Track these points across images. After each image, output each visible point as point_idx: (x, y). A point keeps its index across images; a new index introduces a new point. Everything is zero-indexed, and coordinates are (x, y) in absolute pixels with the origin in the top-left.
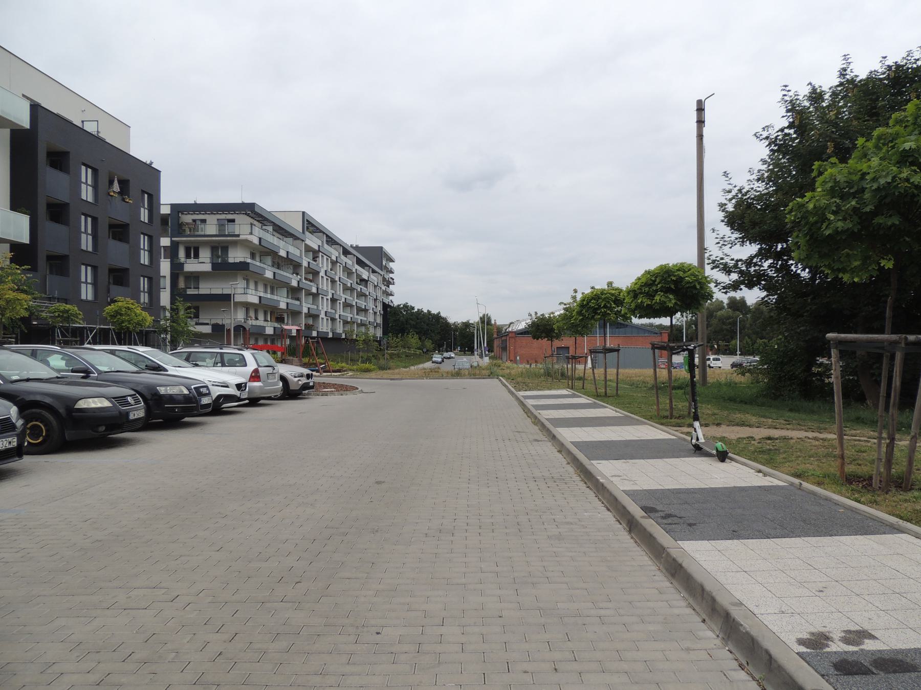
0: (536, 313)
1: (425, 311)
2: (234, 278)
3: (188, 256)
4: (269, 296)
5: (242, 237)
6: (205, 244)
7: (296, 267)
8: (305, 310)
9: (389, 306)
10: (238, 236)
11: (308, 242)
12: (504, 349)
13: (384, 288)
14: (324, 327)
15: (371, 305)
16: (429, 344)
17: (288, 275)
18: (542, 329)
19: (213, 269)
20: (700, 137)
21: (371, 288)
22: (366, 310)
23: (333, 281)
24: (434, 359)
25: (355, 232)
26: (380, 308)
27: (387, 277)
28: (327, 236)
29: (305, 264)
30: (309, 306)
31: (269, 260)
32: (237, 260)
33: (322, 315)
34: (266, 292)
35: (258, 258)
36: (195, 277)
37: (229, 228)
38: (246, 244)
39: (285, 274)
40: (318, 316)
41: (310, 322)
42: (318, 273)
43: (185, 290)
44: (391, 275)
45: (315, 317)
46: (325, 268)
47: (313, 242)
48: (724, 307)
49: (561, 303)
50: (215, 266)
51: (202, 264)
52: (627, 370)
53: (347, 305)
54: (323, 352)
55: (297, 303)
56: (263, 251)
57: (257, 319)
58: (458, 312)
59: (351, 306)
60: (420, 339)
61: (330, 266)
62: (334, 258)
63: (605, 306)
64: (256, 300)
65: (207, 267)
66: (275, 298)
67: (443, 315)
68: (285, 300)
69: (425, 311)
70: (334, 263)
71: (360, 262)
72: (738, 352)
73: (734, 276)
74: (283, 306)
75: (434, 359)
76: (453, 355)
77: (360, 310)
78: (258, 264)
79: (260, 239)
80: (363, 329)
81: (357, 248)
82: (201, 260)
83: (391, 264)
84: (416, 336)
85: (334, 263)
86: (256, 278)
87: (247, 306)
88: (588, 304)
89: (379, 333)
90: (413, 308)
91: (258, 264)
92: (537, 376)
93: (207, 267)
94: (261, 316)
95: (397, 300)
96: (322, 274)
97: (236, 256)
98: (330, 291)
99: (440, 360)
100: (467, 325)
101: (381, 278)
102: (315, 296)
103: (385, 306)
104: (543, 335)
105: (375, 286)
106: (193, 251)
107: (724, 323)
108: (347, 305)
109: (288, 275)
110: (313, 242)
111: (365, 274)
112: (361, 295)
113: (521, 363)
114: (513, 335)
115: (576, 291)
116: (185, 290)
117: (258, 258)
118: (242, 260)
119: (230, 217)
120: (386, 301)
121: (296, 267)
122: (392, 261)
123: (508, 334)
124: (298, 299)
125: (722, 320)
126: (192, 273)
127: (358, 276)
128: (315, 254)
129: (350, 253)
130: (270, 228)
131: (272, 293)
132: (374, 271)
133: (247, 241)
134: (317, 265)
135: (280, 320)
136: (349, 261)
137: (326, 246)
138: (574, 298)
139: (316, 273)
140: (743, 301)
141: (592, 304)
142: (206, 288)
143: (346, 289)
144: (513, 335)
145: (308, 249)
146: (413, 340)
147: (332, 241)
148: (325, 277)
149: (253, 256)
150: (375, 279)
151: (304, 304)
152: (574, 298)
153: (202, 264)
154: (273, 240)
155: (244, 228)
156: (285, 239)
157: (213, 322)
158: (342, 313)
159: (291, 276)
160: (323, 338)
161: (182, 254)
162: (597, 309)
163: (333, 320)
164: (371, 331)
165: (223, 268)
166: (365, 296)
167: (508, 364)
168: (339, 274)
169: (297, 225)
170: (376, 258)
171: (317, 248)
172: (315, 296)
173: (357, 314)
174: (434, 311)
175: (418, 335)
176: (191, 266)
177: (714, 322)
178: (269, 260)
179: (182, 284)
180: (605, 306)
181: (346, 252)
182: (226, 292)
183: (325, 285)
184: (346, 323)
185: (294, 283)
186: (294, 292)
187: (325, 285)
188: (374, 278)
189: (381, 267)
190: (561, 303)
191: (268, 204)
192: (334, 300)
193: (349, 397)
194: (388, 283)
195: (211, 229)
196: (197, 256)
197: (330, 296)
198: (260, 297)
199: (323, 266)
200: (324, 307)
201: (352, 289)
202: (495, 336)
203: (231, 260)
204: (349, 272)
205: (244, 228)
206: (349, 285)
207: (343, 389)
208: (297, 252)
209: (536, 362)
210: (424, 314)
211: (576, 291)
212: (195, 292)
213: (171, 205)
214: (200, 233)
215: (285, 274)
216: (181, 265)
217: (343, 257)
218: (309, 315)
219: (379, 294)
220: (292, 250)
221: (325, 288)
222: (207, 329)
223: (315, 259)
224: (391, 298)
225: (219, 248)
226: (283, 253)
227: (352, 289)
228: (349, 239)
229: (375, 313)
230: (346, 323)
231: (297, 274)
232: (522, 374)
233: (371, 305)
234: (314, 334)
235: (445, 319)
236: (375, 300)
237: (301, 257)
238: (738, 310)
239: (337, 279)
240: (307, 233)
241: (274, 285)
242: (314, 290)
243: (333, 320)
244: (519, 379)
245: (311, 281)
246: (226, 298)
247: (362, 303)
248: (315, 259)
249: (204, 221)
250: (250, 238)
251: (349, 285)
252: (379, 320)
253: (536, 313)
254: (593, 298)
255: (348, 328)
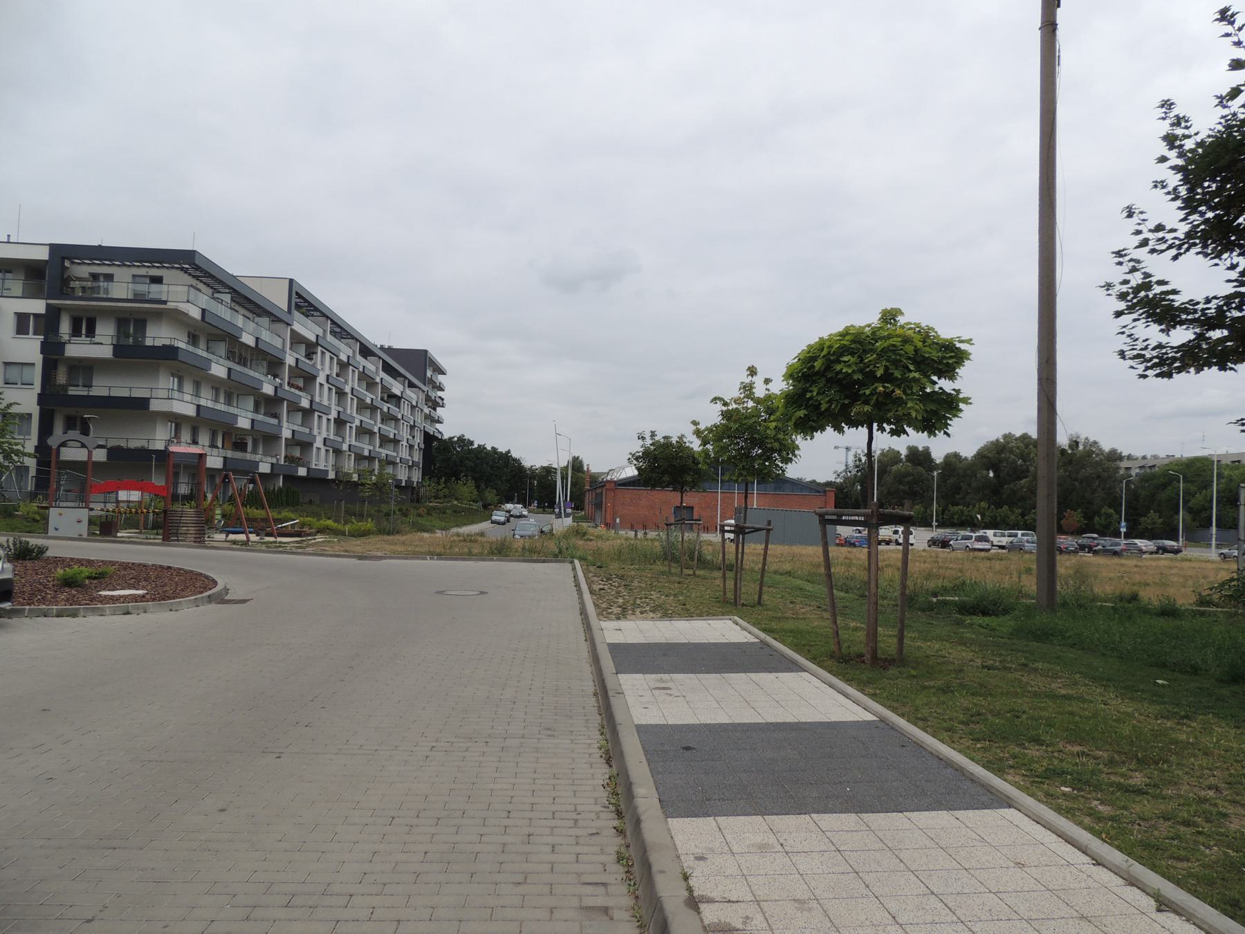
0: (653, 434)
1: (489, 448)
2: (152, 371)
3: (76, 332)
4: (221, 407)
5: (170, 305)
6: (107, 313)
7: (274, 365)
8: (286, 433)
9: (433, 438)
10: (165, 302)
11: (297, 327)
12: (598, 505)
13: (427, 410)
14: (322, 461)
15: (404, 434)
16: (490, 495)
17: (256, 375)
18: (665, 466)
19: (115, 354)
20: (1049, 27)
21: (405, 410)
22: (396, 442)
23: (341, 394)
24: (494, 518)
25: (382, 321)
26: (418, 440)
27: (432, 394)
28: (333, 322)
29: (290, 360)
30: (296, 428)
31: (222, 348)
32: (159, 343)
33: (319, 443)
34: (216, 401)
35: (202, 344)
36: (85, 368)
37: (155, 290)
38: (177, 317)
39: (252, 373)
40: (310, 445)
41: (297, 453)
42: (314, 378)
43: (64, 388)
44: (440, 393)
45: (306, 445)
46: (327, 372)
47: (308, 329)
48: (901, 460)
49: (715, 400)
50: (118, 349)
51: (100, 346)
52: (794, 548)
53: (363, 431)
54: (298, 501)
55: (274, 421)
56: (209, 332)
57: (195, 442)
58: (534, 454)
59: (371, 433)
60: (478, 487)
61: (336, 369)
62: (343, 358)
63: (887, 377)
64: (190, 411)
65: (106, 352)
66: (232, 410)
67: (514, 454)
68: (250, 415)
69: (489, 448)
70: (344, 366)
71: (388, 369)
72: (934, 523)
73: (1182, 335)
74: (244, 423)
75: (494, 518)
76: (525, 513)
77: (385, 440)
78: (204, 354)
79: (204, 311)
80: (390, 470)
81: (390, 351)
82: (97, 339)
83: (441, 378)
84: (471, 483)
85: (344, 366)
86: (195, 375)
87: (177, 421)
88: (828, 366)
89: (416, 476)
90: (472, 443)
91: (204, 354)
92: (648, 558)
93: (106, 352)
94: (204, 439)
95: (449, 429)
96: (321, 379)
97: (158, 335)
98: (333, 407)
99: (502, 519)
100: (548, 471)
101: (422, 396)
102: (307, 413)
103: (429, 438)
104: (666, 478)
105: (413, 407)
106: (85, 325)
107: (901, 482)
108: (363, 431)
109: (256, 375)
110: (308, 329)
111: (397, 388)
112: (388, 418)
113: (623, 528)
114: (612, 486)
115: (752, 371)
116: (64, 388)
117: (202, 344)
118: (167, 342)
119: (154, 272)
120: (431, 430)
121: (274, 365)
122: (442, 373)
123: (604, 484)
124: (275, 416)
125: (900, 478)
126: (80, 360)
127: (385, 389)
128: (311, 349)
129: (373, 354)
130: (227, 298)
131: (229, 402)
132: (411, 385)
133: (177, 312)
134: (314, 366)
135: (240, 446)
136: (371, 366)
137: (329, 338)
138: (748, 389)
139: (310, 378)
140: (927, 453)
141: (848, 365)
142: (102, 387)
143: (362, 406)
144: (612, 486)
145: (297, 339)
146: (466, 488)
147: (342, 331)
148: (326, 386)
149: (193, 339)
150: (414, 396)
151: (285, 424)
152: (748, 389)
153: (100, 346)
154: (224, 311)
155: (180, 294)
156: (257, 319)
157: (112, 443)
158: (353, 443)
159: (262, 378)
160: (317, 480)
161: (65, 327)
162: (862, 384)
163: (338, 452)
164: (402, 475)
165: (134, 354)
166: (396, 420)
167: (601, 530)
168: (351, 382)
169: (279, 299)
170: (417, 366)
171: (313, 339)
172: (307, 413)
173: (381, 446)
174: (502, 449)
175: (473, 479)
176: (77, 349)
177: (888, 479)
178: (222, 348)
179: (61, 378)
180: (887, 377)
181: (366, 351)
182: (137, 393)
183: (325, 397)
184: (360, 458)
185: (268, 389)
186: (269, 404)
187: (325, 397)
188: (411, 395)
189: (424, 379)
190: (715, 400)
191: (232, 259)
192: (340, 423)
193: (187, 616)
194: (435, 404)
195: (122, 287)
196: (91, 332)
197: (333, 415)
198: (198, 406)
199: (324, 368)
200: (322, 431)
201: (373, 408)
202: (587, 487)
203: (149, 342)
204: (364, 377)
205: (180, 294)
206: (368, 401)
207: (169, 586)
208: (278, 343)
209: (645, 527)
210: (488, 453)
211: (752, 371)
212: (81, 391)
213: (51, 246)
214: (102, 295)
215: (252, 373)
216: (61, 346)
217: (359, 358)
218: (294, 442)
219: (419, 419)
220: (266, 336)
221: (326, 402)
222: (100, 456)
223: (309, 356)
224: (438, 426)
225: (131, 321)
226: (248, 339)
227: (373, 408)
228: (377, 338)
229: (411, 447)
230: (360, 458)
231: (275, 376)
232: (619, 555)
233: (404, 434)
234: (302, 472)
235: (517, 461)
236: (412, 427)
237: (283, 351)
238: (920, 464)
239: (348, 389)
240: (296, 314)
241: (232, 389)
242: (305, 403)
243: (338, 452)
244: (614, 566)
245: (298, 388)
246: (141, 404)
247: (390, 431)
248: (309, 356)
249: (109, 278)
250: (183, 307)
251: (368, 401)
252: (417, 457)
253: (653, 434)
254: (844, 350)
255: (365, 465)
